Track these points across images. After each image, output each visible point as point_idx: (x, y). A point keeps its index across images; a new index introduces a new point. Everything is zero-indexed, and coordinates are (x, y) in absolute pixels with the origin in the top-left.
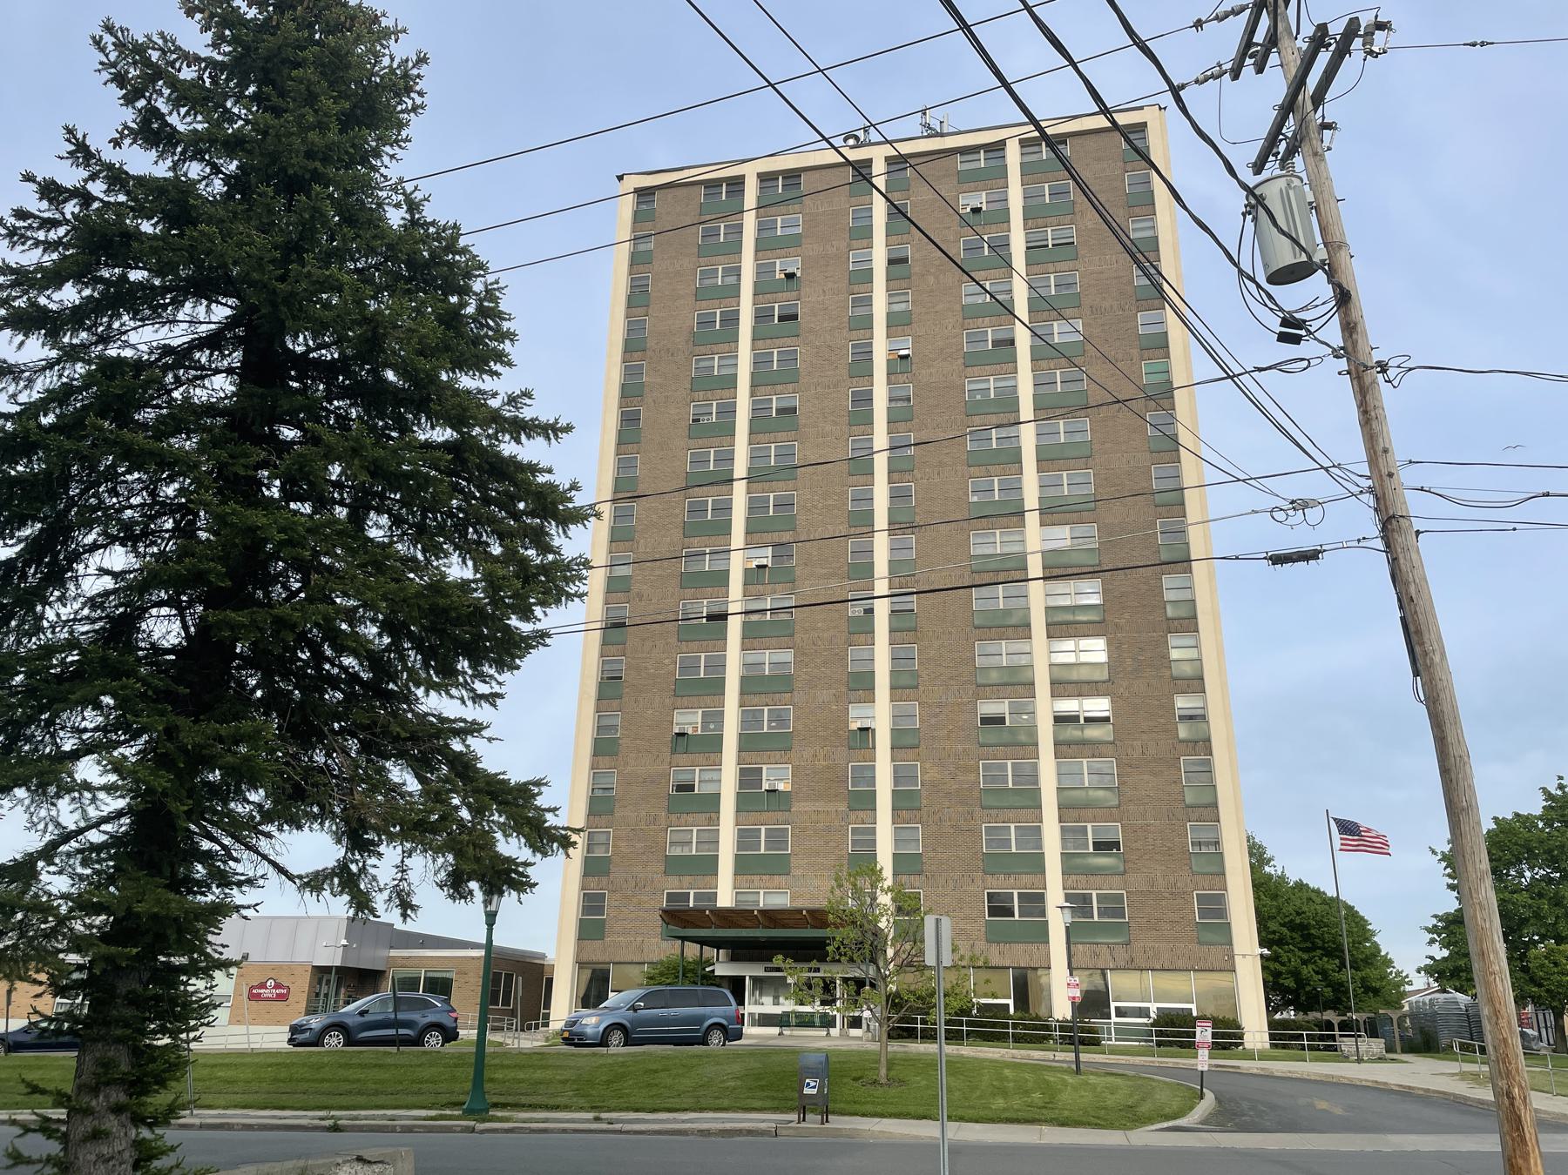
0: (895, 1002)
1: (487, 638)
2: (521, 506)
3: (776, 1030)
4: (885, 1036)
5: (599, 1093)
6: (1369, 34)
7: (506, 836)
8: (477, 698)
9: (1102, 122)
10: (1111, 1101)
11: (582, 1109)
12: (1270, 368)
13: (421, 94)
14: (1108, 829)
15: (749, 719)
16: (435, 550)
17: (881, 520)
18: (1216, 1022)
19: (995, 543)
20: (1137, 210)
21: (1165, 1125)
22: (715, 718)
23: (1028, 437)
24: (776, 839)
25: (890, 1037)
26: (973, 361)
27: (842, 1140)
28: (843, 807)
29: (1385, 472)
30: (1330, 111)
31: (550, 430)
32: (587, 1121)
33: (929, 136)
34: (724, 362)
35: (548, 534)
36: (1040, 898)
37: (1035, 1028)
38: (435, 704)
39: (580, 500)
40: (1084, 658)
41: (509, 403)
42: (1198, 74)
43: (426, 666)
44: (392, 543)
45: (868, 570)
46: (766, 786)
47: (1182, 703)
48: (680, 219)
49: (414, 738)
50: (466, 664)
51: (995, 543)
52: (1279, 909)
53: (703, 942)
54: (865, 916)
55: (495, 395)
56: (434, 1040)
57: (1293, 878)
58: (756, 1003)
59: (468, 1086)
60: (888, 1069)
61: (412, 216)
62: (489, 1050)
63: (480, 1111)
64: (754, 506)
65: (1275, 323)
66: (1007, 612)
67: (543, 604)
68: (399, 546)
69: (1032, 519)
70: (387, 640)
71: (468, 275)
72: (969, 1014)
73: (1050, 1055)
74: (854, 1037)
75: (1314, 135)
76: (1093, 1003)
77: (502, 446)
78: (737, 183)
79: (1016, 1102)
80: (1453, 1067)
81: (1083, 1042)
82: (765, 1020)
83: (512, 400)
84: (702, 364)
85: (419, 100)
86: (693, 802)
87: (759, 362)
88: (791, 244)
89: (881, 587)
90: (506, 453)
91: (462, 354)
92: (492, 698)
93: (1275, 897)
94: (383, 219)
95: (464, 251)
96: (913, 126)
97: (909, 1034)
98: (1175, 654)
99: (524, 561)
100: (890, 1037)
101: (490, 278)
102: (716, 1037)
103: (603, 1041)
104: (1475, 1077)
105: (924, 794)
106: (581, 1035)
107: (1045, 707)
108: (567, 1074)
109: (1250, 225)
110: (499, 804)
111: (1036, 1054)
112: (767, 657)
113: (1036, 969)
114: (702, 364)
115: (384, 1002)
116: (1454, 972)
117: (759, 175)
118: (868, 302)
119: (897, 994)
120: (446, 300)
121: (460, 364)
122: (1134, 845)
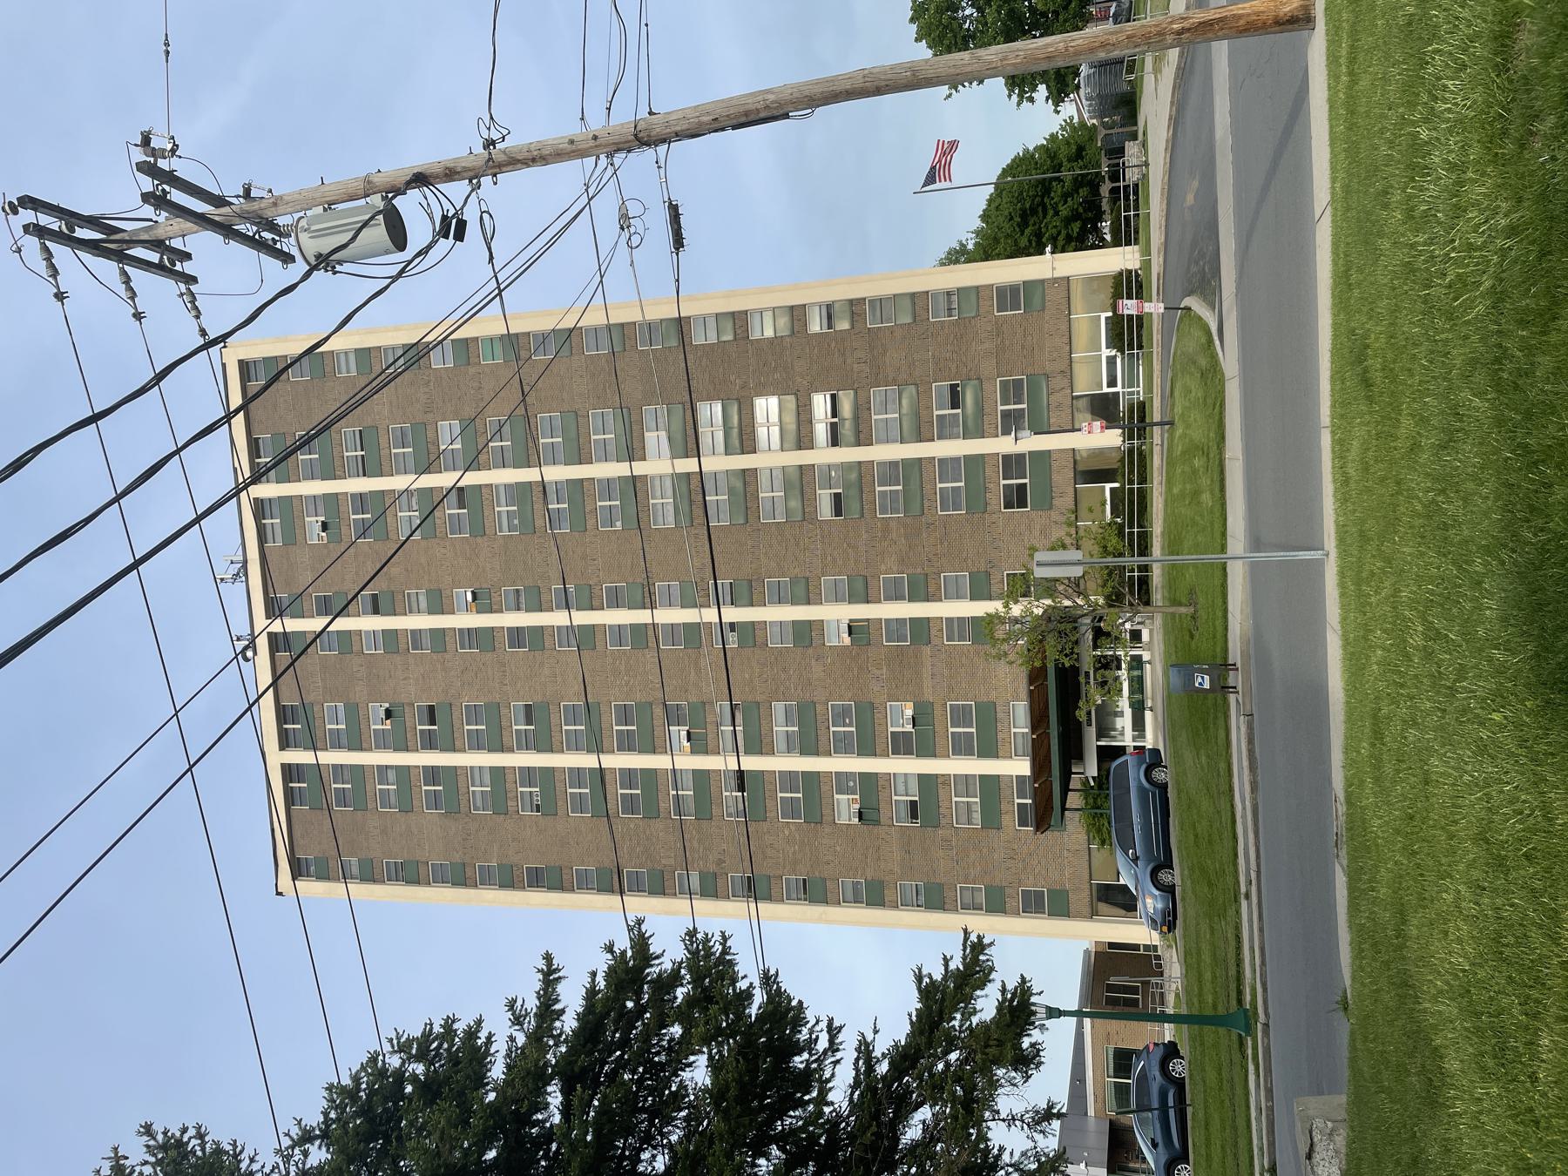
0: (1115, 599)
1: (770, 1039)
2: (630, 1004)
3: (1148, 714)
4: (1148, 608)
5: (1221, 896)
6: (154, 153)
7: (975, 1012)
8: (833, 1047)
9: (239, 420)
10: (1197, 392)
11: (1238, 912)
12: (490, 249)
13: (184, 1130)
14: (939, 395)
15: (843, 746)
16: (678, 1098)
17: (642, 616)
18: (1117, 295)
19: (663, 504)
20: (327, 369)
21: (1217, 343)
22: (843, 781)
23: (556, 473)
24: (961, 716)
25: (1147, 603)
26: (479, 528)
27: (1252, 652)
28: (927, 650)
29: (592, 143)
30: (231, 190)
31: (550, 977)
32: (1250, 906)
33: (246, 575)
34: (478, 782)
35: (660, 975)
36: (1007, 459)
37: (1131, 463)
38: (840, 1095)
39: (623, 943)
40: (774, 417)
41: (521, 1024)
42: (190, 316)
43: (803, 1104)
44: (671, 1146)
45: (692, 630)
46: (909, 728)
47: (816, 326)
48: (326, 833)
49: (876, 1117)
50: (797, 1059)
51: (663, 504)
52: (1007, 236)
53: (1065, 790)
54: (1032, 630)
55: (512, 1039)
56: (1178, 1068)
57: (978, 223)
58: (1122, 734)
59: (1222, 1031)
60: (1180, 604)
61: (317, 1137)
62: (1184, 1011)
63: (1246, 1017)
64: (627, 744)
65: (444, 244)
66: (731, 491)
67: (734, 981)
68: (674, 1138)
69: (640, 468)
70: (775, 1151)
71: (382, 1073)
72: (1121, 526)
73: (1157, 450)
74: (1150, 642)
75: (255, 206)
76: (1104, 408)
77: (567, 1030)
78: (289, 772)
79: (1205, 481)
80: (1149, 81)
81: (1142, 418)
82: (1139, 724)
83: (518, 1021)
84: (479, 803)
85: (191, 1132)
86: (927, 801)
87: (477, 744)
88: (355, 715)
89: (710, 615)
90: (575, 1024)
91: (468, 1077)
92: (833, 1031)
93: (996, 240)
94: (320, 1167)
95: (356, 1079)
96: (234, 594)
97: (1144, 583)
98: (769, 333)
99: (690, 1001)
100: (1147, 603)
101: (387, 1047)
102: (1159, 775)
103: (1169, 890)
104: (1158, 62)
105: (910, 571)
106: (1165, 913)
107: (823, 455)
108: (1204, 927)
109: (346, 267)
110: (941, 1020)
111: (1157, 462)
112: (780, 729)
113: (1075, 462)
114: (479, 803)
115: (1142, 1122)
116: (1061, 84)
117: (282, 748)
118: (416, 633)
119: (1108, 598)
120: (410, 1098)
121: (479, 1080)
122: (954, 370)
